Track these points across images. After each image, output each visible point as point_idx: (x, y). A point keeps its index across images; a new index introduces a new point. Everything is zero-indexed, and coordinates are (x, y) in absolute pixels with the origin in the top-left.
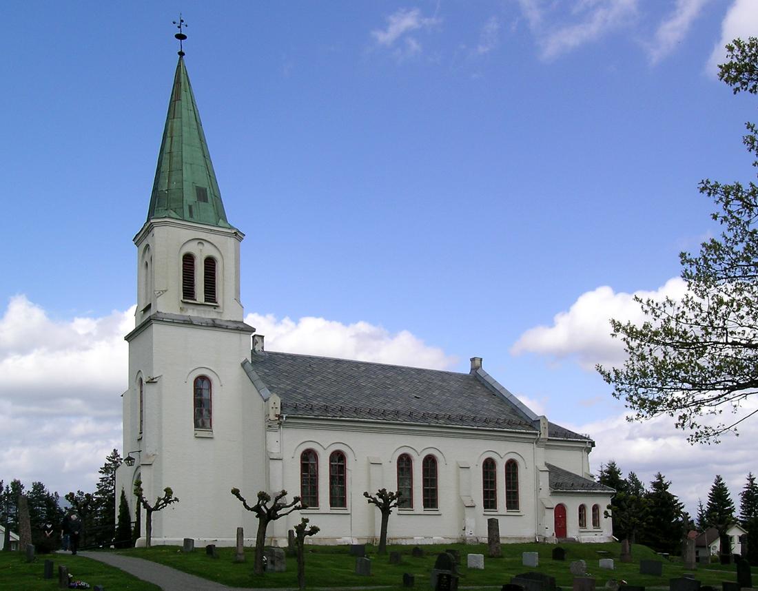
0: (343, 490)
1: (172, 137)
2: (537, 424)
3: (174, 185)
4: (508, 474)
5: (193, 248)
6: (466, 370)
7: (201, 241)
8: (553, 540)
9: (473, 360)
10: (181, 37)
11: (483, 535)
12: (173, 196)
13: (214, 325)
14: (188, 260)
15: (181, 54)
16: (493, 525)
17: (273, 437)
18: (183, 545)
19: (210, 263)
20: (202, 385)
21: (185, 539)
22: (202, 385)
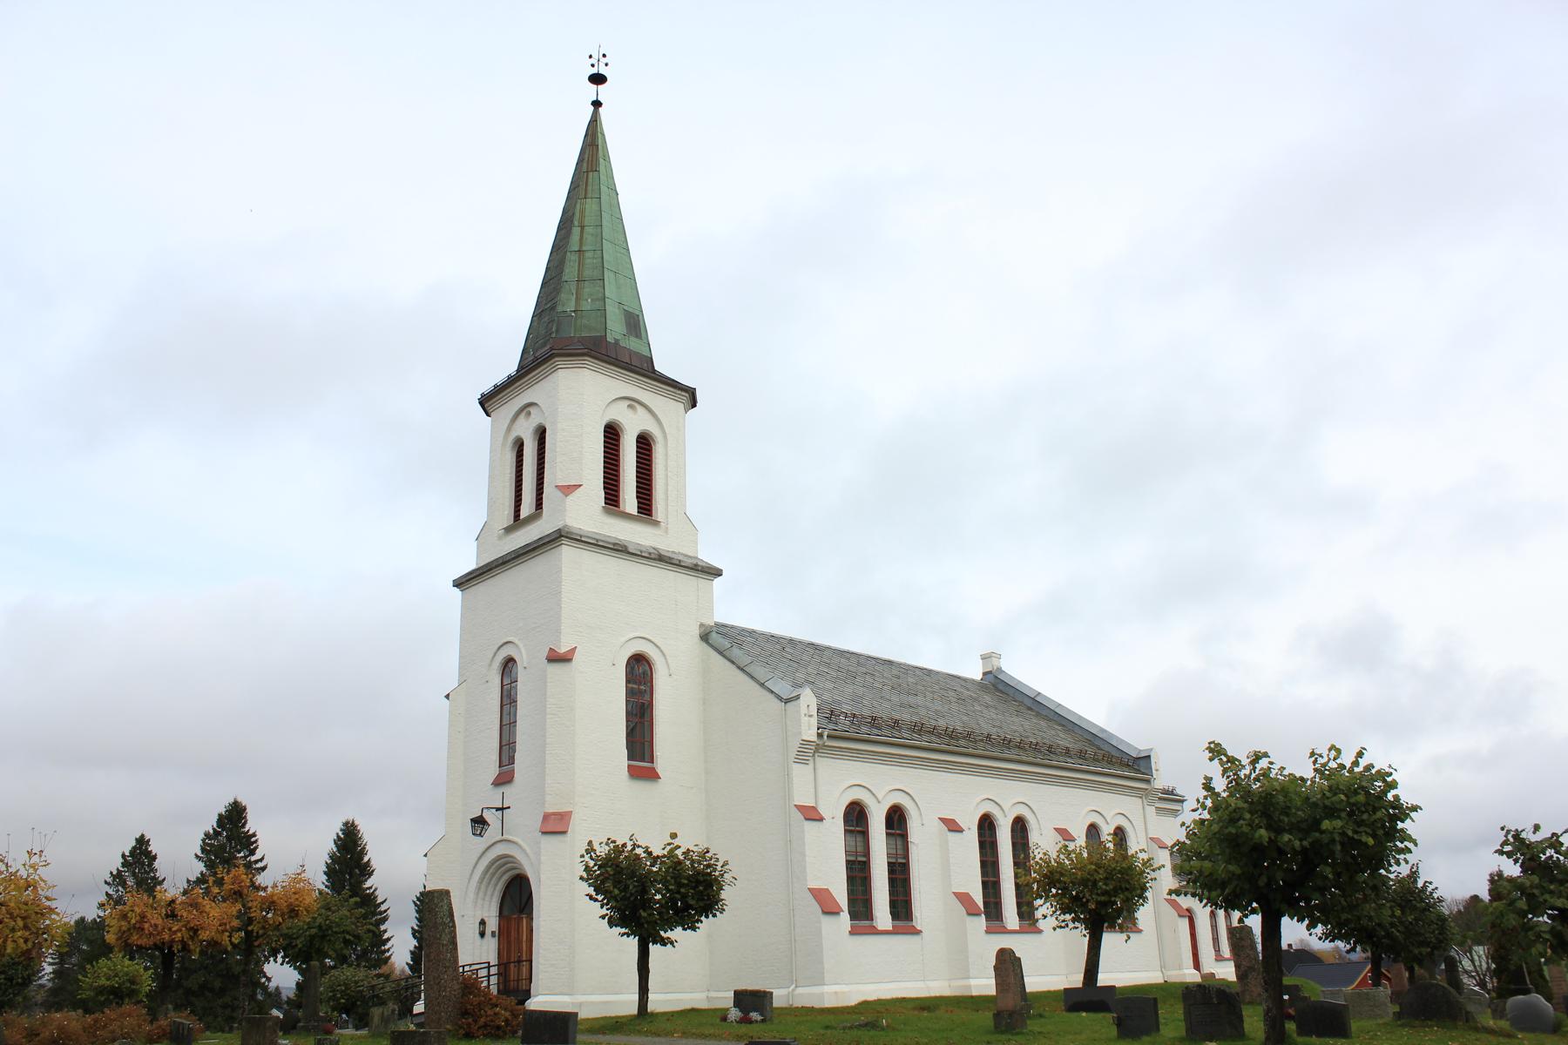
0: (984, 873)
1: (582, 227)
2: (1142, 762)
3: (587, 305)
4: (892, 882)
5: (621, 414)
6: (975, 672)
7: (633, 402)
8: (1191, 976)
9: (985, 658)
10: (598, 79)
11: (984, 983)
12: (585, 321)
13: (661, 559)
14: (612, 434)
15: (597, 104)
16: (1007, 965)
17: (801, 775)
18: (992, 991)
19: (645, 444)
20: (639, 670)
21: (736, 992)
22: (639, 670)
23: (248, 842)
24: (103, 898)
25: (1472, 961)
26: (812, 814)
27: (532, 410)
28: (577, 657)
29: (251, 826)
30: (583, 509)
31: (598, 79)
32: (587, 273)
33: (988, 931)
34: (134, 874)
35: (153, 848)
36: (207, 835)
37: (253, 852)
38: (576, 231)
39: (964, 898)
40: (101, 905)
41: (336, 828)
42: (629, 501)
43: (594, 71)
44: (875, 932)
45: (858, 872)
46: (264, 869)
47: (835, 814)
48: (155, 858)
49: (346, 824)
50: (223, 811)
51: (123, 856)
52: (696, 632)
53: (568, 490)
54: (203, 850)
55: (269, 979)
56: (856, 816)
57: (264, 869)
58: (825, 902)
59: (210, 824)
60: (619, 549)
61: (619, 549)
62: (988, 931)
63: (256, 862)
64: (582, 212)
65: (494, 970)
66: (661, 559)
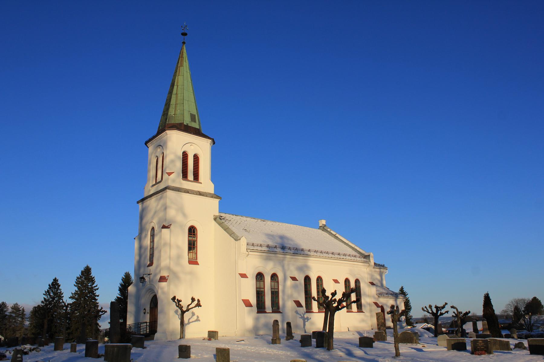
3: (178, 112)
20: (192, 231)
23: (92, 280)
24: (43, 300)
25: (524, 321)
26: (243, 276)
27: (161, 147)
28: (172, 227)
29: (93, 274)
30: (175, 180)
31: (184, 34)
32: (178, 102)
33: (348, 312)
34: (52, 291)
35: (59, 282)
36: (78, 278)
37: (93, 284)
38: (175, 87)
39: (247, 303)
40: (42, 302)
41: (122, 275)
42: (191, 176)
43: (183, 32)
44: (352, 312)
45: (260, 294)
46: (97, 289)
47: (251, 274)
48: (60, 286)
49: (126, 273)
50: (83, 269)
51: (49, 285)
52: (213, 218)
53: (169, 174)
54: (76, 283)
55: (100, 327)
56: (260, 276)
57: (97, 289)
58: (298, 304)
59: (79, 274)
60: (187, 191)
61: (187, 191)
62: (348, 312)
63: (95, 287)
64: (178, 79)
65: (148, 324)
66: (200, 194)
